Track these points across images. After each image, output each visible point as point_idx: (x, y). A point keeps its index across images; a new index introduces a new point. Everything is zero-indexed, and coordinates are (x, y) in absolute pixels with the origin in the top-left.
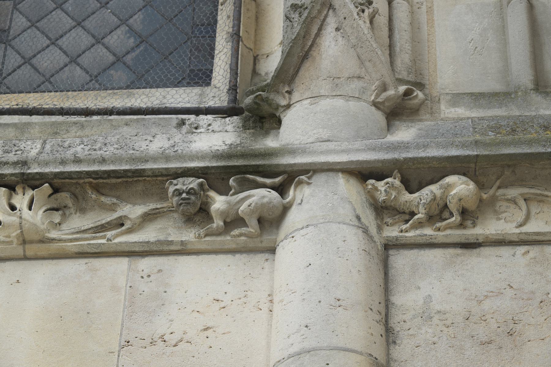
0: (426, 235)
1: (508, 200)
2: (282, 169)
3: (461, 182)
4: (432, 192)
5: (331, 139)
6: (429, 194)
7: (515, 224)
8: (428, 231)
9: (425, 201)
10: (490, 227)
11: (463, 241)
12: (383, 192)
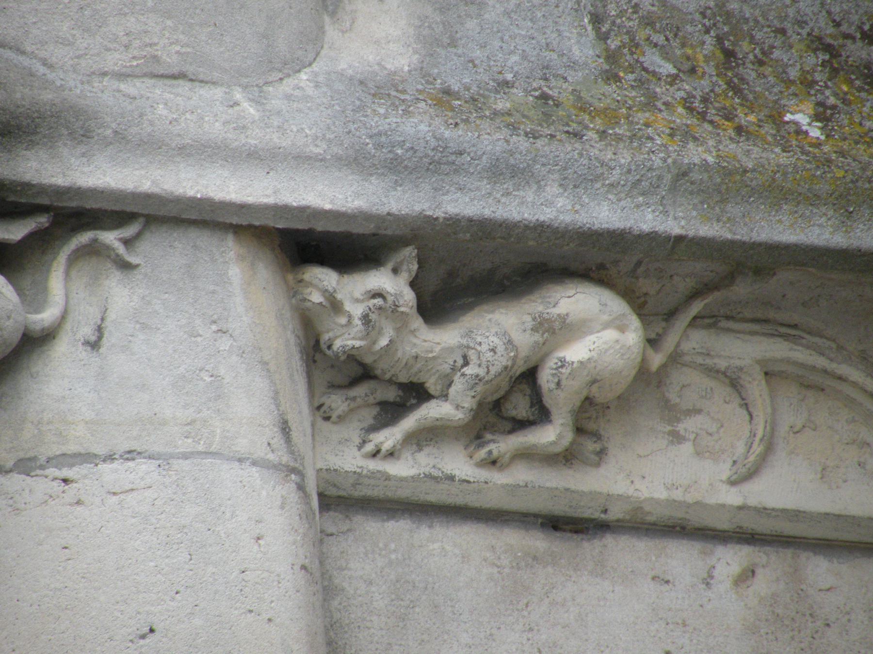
0: (451, 478)
1: (712, 372)
2: (45, 201)
3: (605, 318)
4: (510, 342)
5: (190, 69)
6: (501, 349)
7: (725, 470)
8: (457, 463)
9: (482, 372)
10: (647, 471)
11: (560, 508)
12: (357, 322)
